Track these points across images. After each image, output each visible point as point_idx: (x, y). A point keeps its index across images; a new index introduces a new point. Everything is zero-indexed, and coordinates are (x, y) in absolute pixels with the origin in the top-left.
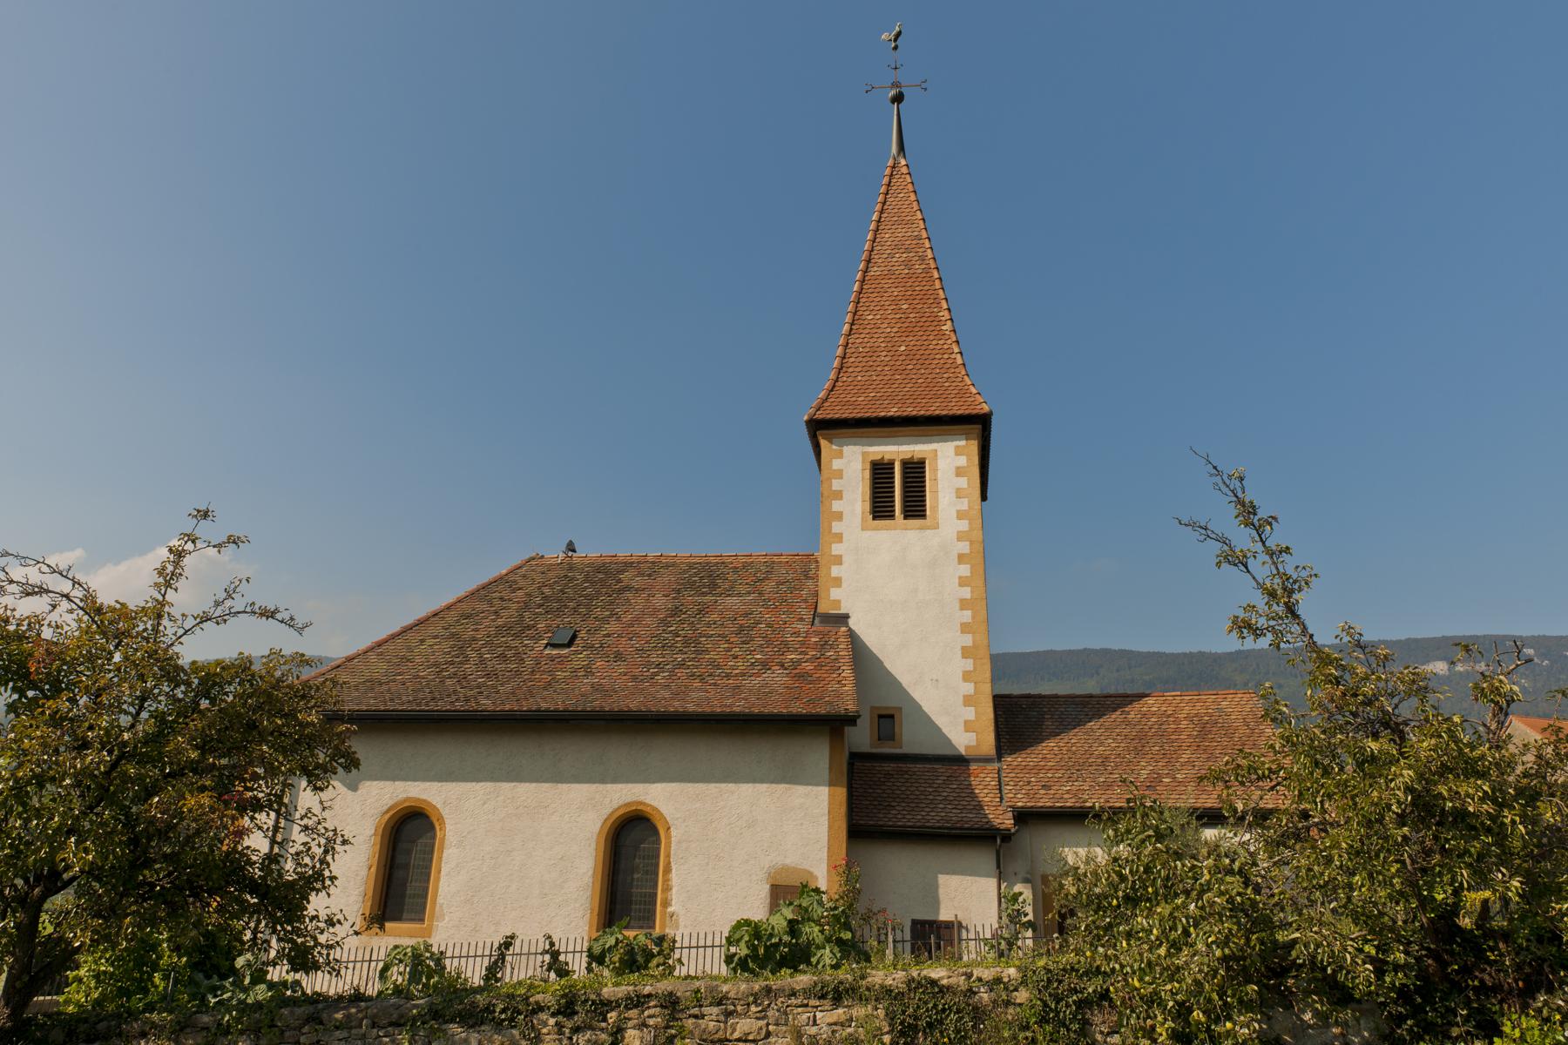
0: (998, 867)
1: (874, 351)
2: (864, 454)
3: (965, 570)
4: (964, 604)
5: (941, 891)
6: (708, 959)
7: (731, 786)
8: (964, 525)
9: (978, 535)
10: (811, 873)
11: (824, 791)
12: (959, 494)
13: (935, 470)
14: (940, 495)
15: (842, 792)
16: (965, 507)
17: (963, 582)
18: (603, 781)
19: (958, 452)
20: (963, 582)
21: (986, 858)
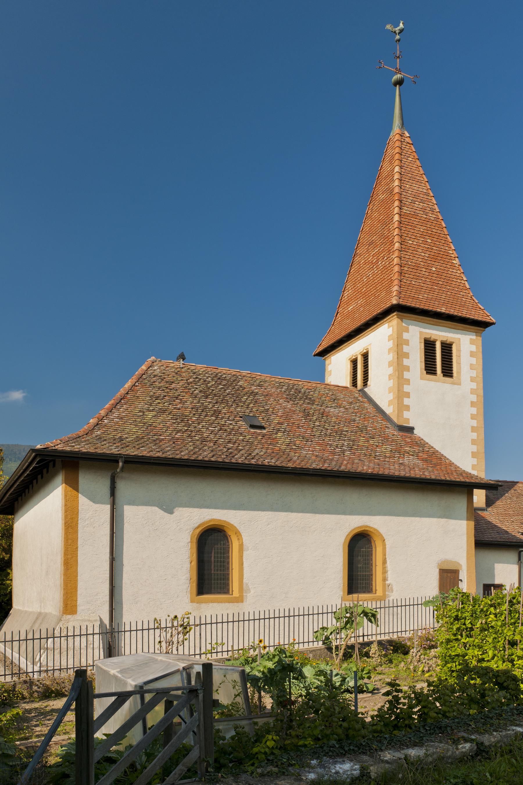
0: (519, 559)
1: (417, 267)
2: (420, 332)
3: (474, 411)
4: (473, 429)
5: (495, 571)
6: (214, 637)
7: (418, 519)
8: (474, 385)
9: (481, 392)
10: (459, 564)
11: (464, 523)
12: (472, 367)
13: (459, 350)
14: (462, 366)
15: (472, 524)
16: (474, 375)
17: (473, 417)
18: (344, 513)
19: (472, 342)
20: (473, 417)
21: (513, 556)
